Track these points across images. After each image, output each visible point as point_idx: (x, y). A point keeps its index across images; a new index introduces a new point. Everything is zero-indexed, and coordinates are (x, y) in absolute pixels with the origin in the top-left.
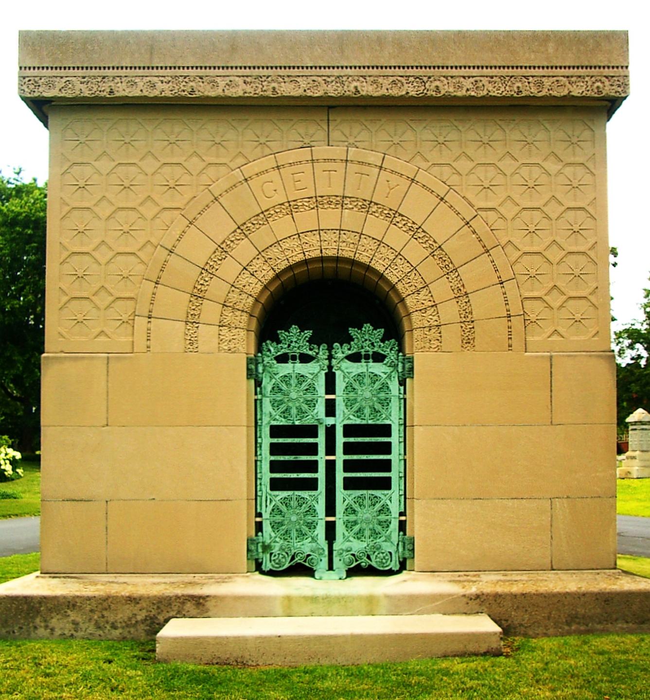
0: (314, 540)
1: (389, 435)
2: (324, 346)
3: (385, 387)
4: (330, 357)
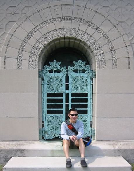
1: (87, 96)
2: (65, 67)
3: (86, 80)
4: (67, 71)
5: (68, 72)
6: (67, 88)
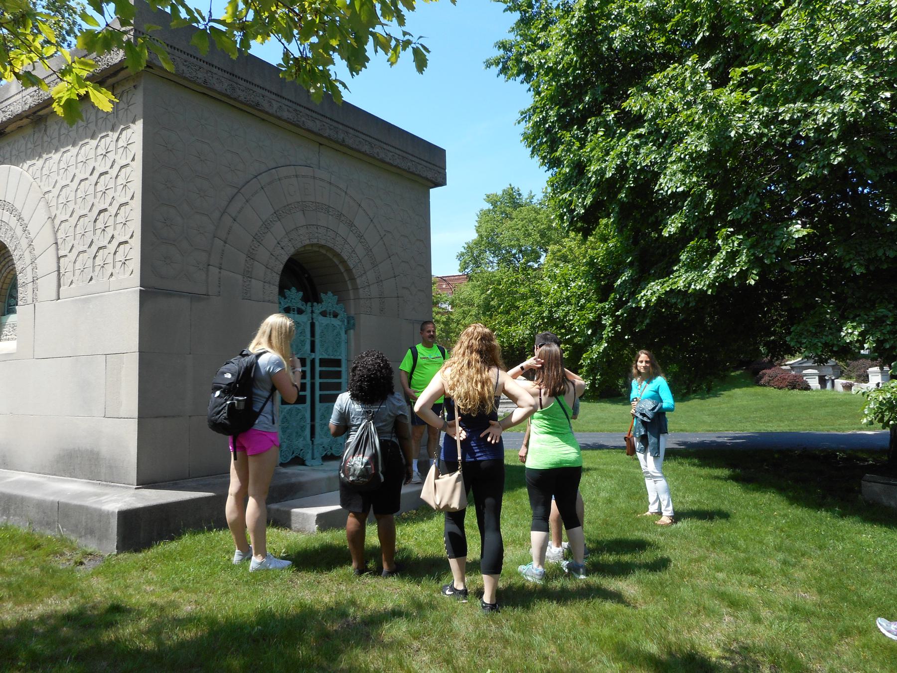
0: (305, 439)
1: (340, 366)
2: (309, 304)
3: (338, 334)
4: (312, 312)
5: (315, 315)
6: (313, 350)
